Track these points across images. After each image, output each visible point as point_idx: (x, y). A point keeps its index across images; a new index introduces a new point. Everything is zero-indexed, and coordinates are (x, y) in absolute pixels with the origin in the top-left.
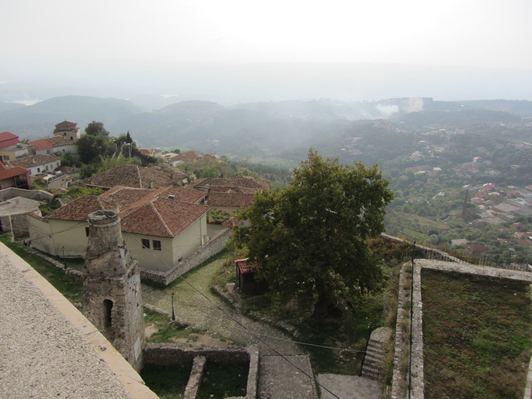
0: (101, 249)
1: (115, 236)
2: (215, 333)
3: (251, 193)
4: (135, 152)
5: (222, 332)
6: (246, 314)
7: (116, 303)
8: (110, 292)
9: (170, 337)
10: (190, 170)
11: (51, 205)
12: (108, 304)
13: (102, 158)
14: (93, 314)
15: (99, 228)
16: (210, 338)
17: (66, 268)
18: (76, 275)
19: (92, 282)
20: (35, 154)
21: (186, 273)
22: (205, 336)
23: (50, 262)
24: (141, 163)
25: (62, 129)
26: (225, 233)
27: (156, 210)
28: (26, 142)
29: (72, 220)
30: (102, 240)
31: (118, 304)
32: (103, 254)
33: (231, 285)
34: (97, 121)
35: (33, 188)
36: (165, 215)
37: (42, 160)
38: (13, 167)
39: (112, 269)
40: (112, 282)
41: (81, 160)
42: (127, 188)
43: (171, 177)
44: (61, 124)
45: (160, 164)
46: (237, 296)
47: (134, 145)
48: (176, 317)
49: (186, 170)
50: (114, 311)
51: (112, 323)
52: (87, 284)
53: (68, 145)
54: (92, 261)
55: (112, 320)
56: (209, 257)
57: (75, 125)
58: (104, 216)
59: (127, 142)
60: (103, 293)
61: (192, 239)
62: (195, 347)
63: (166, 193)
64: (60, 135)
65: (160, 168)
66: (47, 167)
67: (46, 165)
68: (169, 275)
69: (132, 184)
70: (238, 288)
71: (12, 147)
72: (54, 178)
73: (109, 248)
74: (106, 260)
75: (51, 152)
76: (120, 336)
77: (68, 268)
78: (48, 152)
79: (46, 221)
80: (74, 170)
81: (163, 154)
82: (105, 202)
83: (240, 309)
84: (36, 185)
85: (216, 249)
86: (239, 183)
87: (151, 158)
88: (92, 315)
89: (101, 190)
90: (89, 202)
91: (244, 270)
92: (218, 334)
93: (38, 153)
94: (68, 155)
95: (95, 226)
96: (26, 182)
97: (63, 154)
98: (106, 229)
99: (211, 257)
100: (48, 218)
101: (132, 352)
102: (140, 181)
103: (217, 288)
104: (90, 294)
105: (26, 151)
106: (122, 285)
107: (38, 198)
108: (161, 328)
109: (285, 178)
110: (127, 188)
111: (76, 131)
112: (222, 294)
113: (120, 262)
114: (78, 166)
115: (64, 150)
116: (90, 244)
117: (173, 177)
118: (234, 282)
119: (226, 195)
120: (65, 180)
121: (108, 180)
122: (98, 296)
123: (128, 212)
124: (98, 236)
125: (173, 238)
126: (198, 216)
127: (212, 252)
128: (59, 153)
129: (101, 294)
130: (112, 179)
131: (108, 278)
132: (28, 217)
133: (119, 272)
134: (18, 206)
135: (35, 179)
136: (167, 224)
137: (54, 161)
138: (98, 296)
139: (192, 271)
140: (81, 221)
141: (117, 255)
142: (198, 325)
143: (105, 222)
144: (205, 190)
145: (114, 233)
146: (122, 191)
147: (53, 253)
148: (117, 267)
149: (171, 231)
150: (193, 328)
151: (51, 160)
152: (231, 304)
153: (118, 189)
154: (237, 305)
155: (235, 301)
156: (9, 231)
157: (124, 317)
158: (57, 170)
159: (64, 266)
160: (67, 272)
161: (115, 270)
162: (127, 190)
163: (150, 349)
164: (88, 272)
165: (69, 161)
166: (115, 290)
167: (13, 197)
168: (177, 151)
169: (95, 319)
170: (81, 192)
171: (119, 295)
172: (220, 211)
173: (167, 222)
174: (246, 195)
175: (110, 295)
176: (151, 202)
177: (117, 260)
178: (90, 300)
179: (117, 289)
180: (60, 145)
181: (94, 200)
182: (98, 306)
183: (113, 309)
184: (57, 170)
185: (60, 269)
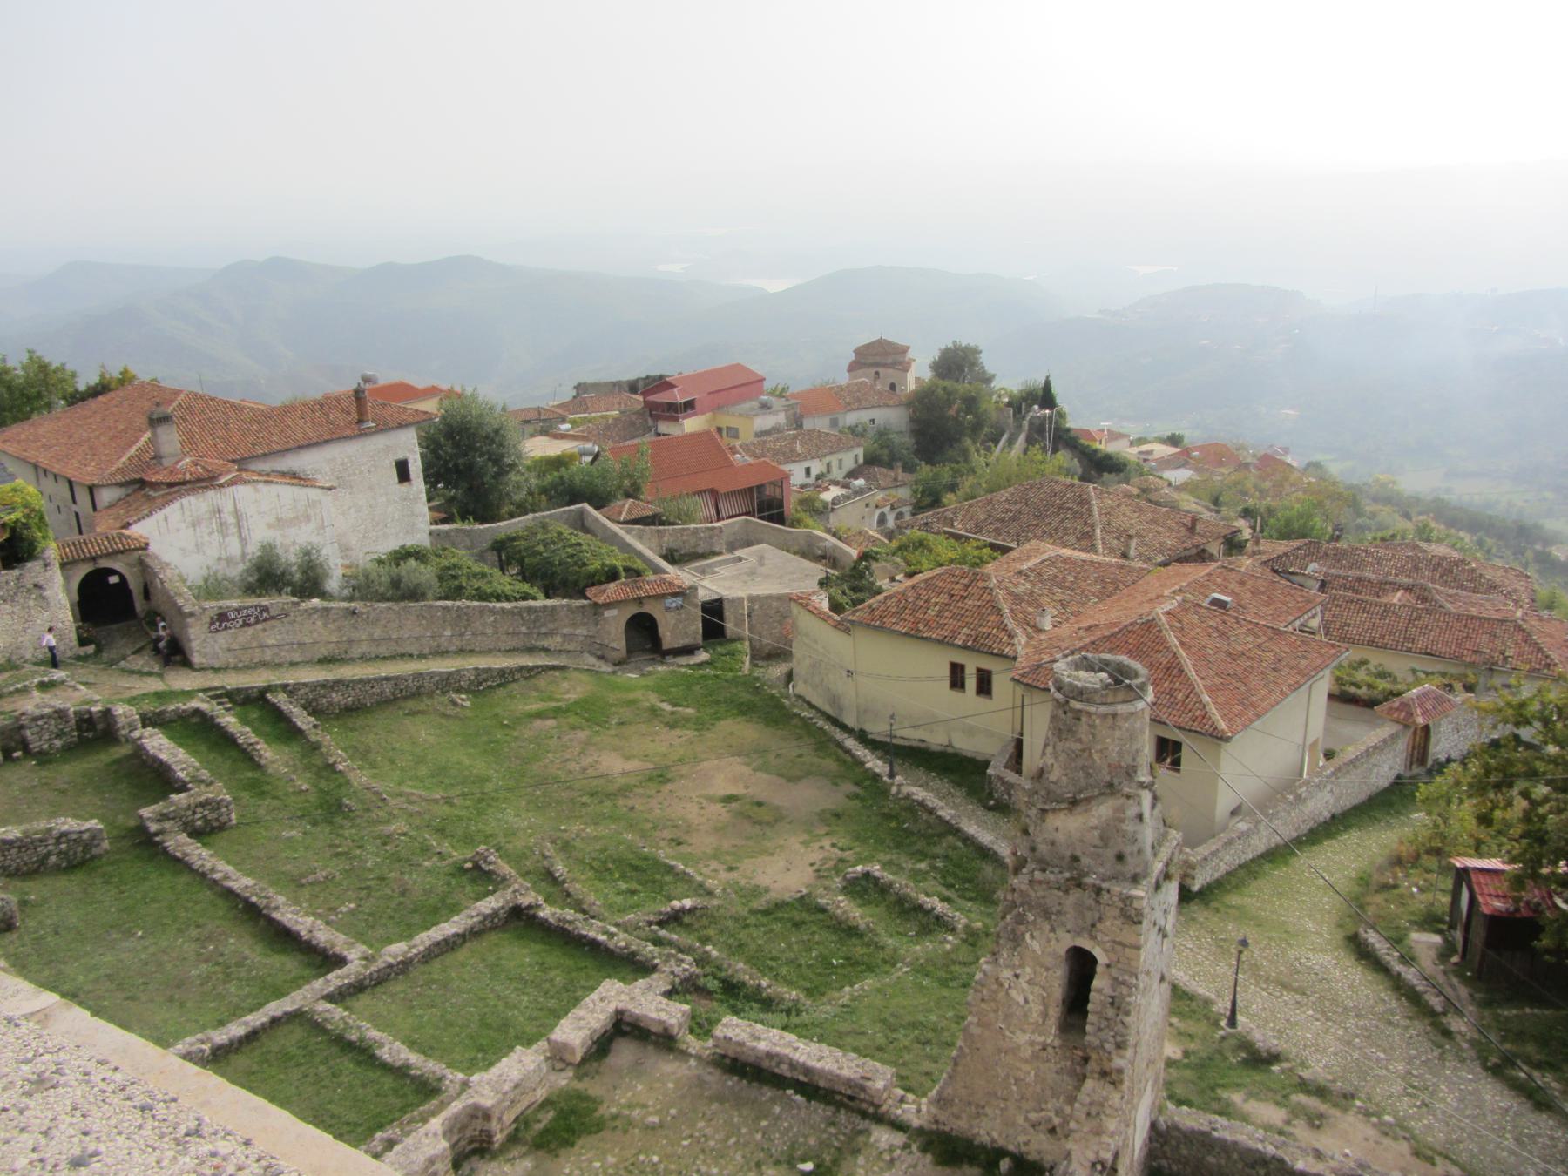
0: (1083, 783)
1: (1135, 747)
2: (1387, 1118)
3: (1474, 611)
4: (1065, 439)
5: (1412, 1117)
6: (1499, 1070)
7: (1108, 966)
8: (1093, 925)
9: (1223, 1086)
10: (1226, 504)
11: (851, 583)
12: (1081, 966)
13: (972, 449)
14: (1028, 982)
15: (1088, 713)
16: (1372, 1133)
17: (892, 775)
18: (922, 804)
19: (1040, 882)
20: (800, 426)
21: (1253, 860)
22: (1350, 1117)
23: (848, 751)
24: (1080, 471)
25: (871, 360)
26: (1384, 741)
27: (1173, 640)
28: (781, 394)
29: (914, 636)
30: (1090, 755)
31: (1114, 972)
32: (1088, 800)
33: (1425, 942)
34: (893, 337)
35: (795, 523)
36: (1201, 658)
37: (820, 445)
38: (749, 460)
39: (1110, 853)
40: (1105, 897)
41: (917, 452)
42: (1067, 552)
43: (1191, 529)
44: (867, 346)
45: (1135, 480)
46: (1455, 989)
47: (1062, 415)
48: (1240, 1018)
49: (1216, 502)
50: (1099, 991)
51: (1088, 1028)
52: (1024, 887)
53: (887, 406)
54: (1050, 818)
55: (1090, 1018)
56: (1327, 815)
57: (904, 350)
58: (1103, 675)
59: (1042, 407)
60: (1069, 926)
61: (1279, 747)
62: (1332, 1164)
63: (1201, 587)
64: (865, 378)
65: (1136, 491)
66: (829, 465)
67: (827, 459)
68: (1205, 859)
69: (1072, 539)
70: (1455, 959)
71: (746, 406)
72: (848, 498)
73: (1111, 785)
74: (1094, 822)
75: (841, 425)
76: (1104, 1074)
77: (898, 778)
78: (834, 423)
79: (845, 628)
80: (895, 480)
81: (1132, 444)
82: (1011, 594)
83: (1472, 1042)
84: (802, 515)
85: (1352, 791)
86: (1416, 568)
87: (1108, 457)
88: (1025, 986)
89: (987, 551)
90: (967, 587)
91: (1494, 905)
92: (1400, 1124)
93: (808, 424)
94: (882, 434)
95: (1078, 705)
96: (780, 504)
97: (871, 433)
98: (1110, 720)
99: (1333, 817)
100: (852, 622)
101: (1130, 1131)
102: (1098, 531)
103: (1372, 937)
104: (1031, 917)
105: (781, 419)
106: (1139, 913)
107: (810, 552)
108: (1192, 1046)
109: (1529, 554)
110: (1067, 552)
111: (905, 367)
112: (1398, 967)
113: (1139, 837)
114: (909, 468)
115: (873, 421)
116: (1050, 761)
117: (1198, 528)
118: (1439, 932)
119: (1387, 609)
120: (873, 505)
121: (1002, 520)
122: (1053, 930)
123: (1082, 633)
124: (1080, 740)
125: (1227, 740)
126: (1307, 676)
127: (1337, 800)
128: (860, 429)
129: (1063, 924)
130: (1013, 519)
131: (1091, 879)
132: (795, 609)
133: (1131, 866)
134: (763, 570)
135: (799, 496)
136: (1209, 689)
137: (848, 449)
138: (1053, 930)
139: (1276, 855)
140: (941, 642)
141: (1131, 811)
142: (1317, 1069)
143: (1110, 699)
144: (1310, 582)
145: (1132, 737)
146: (1052, 562)
147: (850, 721)
148: (1127, 850)
149: (1223, 716)
150: (1306, 1074)
151: (838, 447)
152: (1430, 1013)
153: (1037, 551)
154: (1457, 1024)
155: (1451, 1006)
156: (740, 639)
157: (1127, 1020)
158: (853, 474)
159: (887, 769)
160: (894, 789)
161: (1120, 857)
162: (1067, 560)
163: (1176, 1127)
164: (1033, 849)
165: (886, 451)
166: (1111, 925)
167: (749, 544)
168: (1174, 440)
169: (1031, 998)
170: (930, 551)
171: (1120, 943)
172: (1364, 662)
173: (1209, 683)
174: (1459, 618)
175: (1093, 937)
176: (1160, 611)
177: (1129, 827)
178: (1027, 936)
179: (1118, 922)
180: (864, 404)
181: (980, 584)
182: (1048, 961)
183: (1096, 983)
184: (853, 474)
185: (876, 777)
